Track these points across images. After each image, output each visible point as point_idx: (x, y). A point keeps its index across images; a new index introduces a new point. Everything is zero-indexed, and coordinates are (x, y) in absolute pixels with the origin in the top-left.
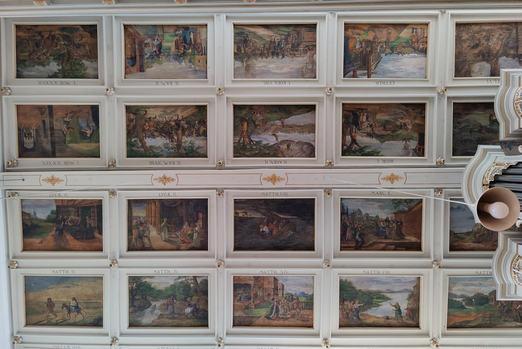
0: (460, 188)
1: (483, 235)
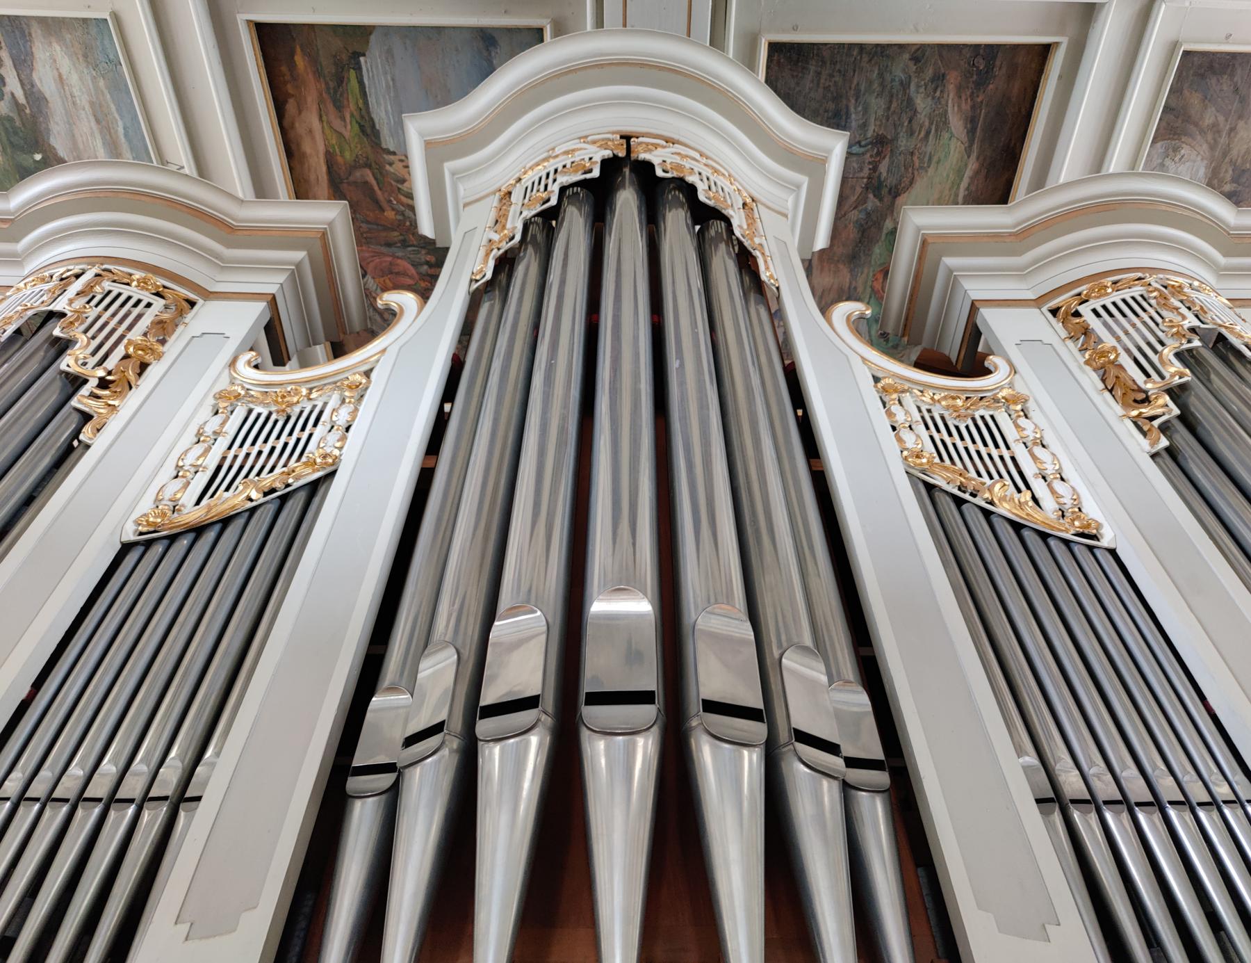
0: (599, 22)
1: (377, 202)
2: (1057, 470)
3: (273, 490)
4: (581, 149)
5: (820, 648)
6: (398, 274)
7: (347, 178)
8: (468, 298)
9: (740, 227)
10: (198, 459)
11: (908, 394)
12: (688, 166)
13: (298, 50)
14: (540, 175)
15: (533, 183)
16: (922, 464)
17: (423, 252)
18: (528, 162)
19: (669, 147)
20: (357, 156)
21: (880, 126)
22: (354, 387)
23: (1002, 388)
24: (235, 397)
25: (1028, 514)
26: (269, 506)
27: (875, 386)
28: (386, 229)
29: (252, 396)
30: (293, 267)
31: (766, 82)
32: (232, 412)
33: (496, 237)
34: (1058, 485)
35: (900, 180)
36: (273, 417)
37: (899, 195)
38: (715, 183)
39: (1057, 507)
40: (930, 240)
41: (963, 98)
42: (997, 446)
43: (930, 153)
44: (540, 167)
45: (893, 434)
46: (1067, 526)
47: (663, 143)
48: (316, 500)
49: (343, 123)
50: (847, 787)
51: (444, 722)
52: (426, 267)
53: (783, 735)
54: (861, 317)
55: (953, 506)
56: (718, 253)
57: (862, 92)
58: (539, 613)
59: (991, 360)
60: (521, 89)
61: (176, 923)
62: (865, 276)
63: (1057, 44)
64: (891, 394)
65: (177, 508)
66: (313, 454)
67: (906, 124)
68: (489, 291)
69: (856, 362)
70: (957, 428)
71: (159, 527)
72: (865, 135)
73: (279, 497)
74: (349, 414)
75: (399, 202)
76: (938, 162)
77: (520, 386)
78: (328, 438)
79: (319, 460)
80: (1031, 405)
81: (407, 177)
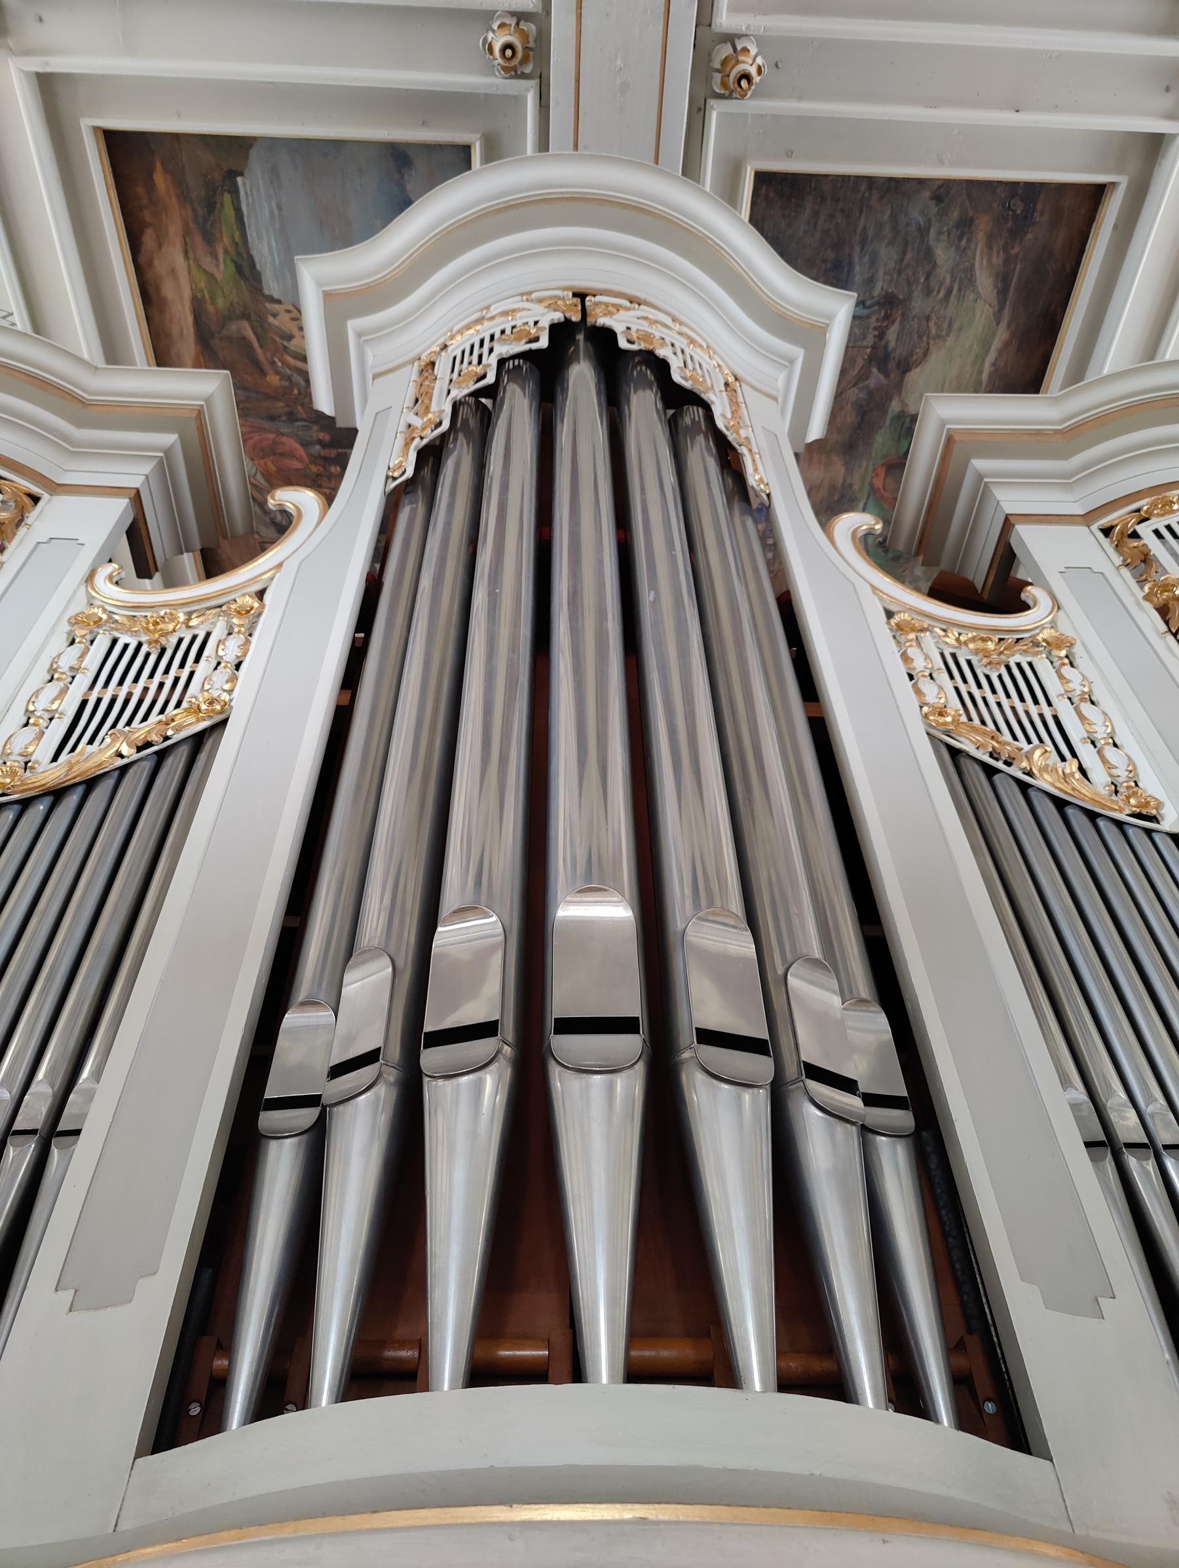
0: (543, 144)
1: (256, 363)
2: (1108, 734)
3: (148, 745)
4: (523, 309)
5: (831, 961)
6: (282, 455)
7: (219, 332)
8: (384, 499)
9: (724, 416)
10: (52, 702)
11: (928, 633)
12: (658, 335)
13: (158, 166)
14: (471, 342)
15: (463, 352)
16: (945, 724)
17: (315, 428)
18: (457, 323)
19: (634, 309)
20: (232, 304)
21: (891, 281)
22: (244, 612)
23: (1042, 627)
24: (95, 623)
25: (1074, 789)
26: (144, 763)
27: (888, 623)
28: (268, 397)
29: (117, 621)
30: (161, 454)
31: (751, 221)
32: (92, 642)
33: (417, 422)
34: (1110, 752)
35: (912, 352)
36: (144, 649)
37: (910, 370)
38: (691, 357)
39: (1109, 780)
40: (957, 438)
41: (995, 249)
42: (1036, 702)
43: (951, 320)
44: (471, 331)
45: (910, 684)
46: (1121, 803)
47: (626, 303)
48: (202, 757)
49: (214, 261)
50: (866, 1131)
51: (380, 1048)
52: (318, 447)
53: (791, 1070)
54: (869, 534)
55: (982, 776)
56: (695, 449)
57: (870, 238)
58: (494, 918)
59: (1029, 592)
60: (446, 228)
61: (56, 1290)
62: (865, 471)
63: (1113, 184)
64: (907, 633)
65: (29, 765)
66: (196, 698)
67: (922, 280)
68: (409, 493)
69: (865, 591)
70: (988, 677)
71: (9, 788)
72: (870, 293)
73: (156, 753)
74: (239, 647)
75: (283, 362)
76: (960, 329)
77: (455, 618)
78: (214, 679)
79: (204, 707)
80: (1078, 650)
81: (296, 332)
